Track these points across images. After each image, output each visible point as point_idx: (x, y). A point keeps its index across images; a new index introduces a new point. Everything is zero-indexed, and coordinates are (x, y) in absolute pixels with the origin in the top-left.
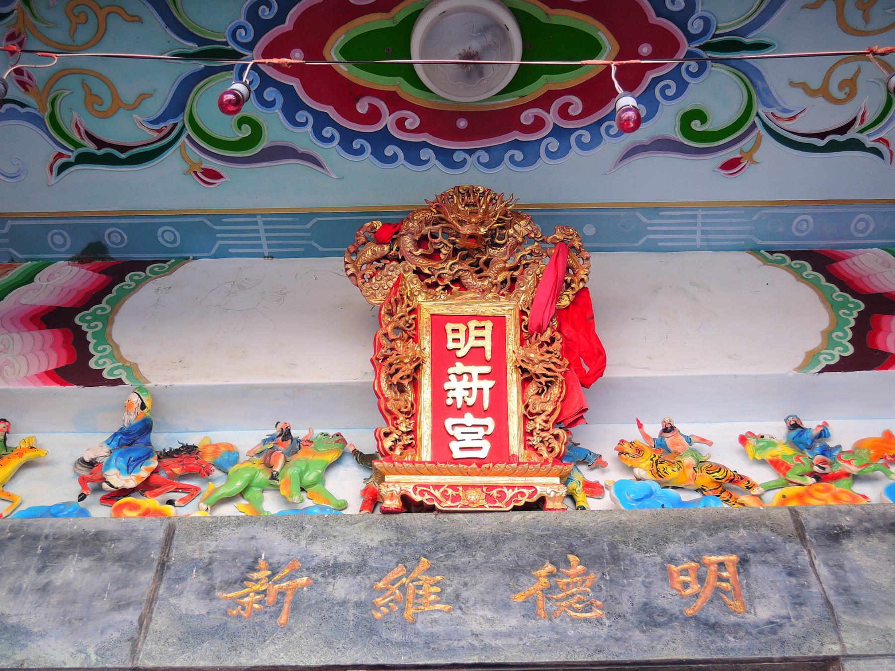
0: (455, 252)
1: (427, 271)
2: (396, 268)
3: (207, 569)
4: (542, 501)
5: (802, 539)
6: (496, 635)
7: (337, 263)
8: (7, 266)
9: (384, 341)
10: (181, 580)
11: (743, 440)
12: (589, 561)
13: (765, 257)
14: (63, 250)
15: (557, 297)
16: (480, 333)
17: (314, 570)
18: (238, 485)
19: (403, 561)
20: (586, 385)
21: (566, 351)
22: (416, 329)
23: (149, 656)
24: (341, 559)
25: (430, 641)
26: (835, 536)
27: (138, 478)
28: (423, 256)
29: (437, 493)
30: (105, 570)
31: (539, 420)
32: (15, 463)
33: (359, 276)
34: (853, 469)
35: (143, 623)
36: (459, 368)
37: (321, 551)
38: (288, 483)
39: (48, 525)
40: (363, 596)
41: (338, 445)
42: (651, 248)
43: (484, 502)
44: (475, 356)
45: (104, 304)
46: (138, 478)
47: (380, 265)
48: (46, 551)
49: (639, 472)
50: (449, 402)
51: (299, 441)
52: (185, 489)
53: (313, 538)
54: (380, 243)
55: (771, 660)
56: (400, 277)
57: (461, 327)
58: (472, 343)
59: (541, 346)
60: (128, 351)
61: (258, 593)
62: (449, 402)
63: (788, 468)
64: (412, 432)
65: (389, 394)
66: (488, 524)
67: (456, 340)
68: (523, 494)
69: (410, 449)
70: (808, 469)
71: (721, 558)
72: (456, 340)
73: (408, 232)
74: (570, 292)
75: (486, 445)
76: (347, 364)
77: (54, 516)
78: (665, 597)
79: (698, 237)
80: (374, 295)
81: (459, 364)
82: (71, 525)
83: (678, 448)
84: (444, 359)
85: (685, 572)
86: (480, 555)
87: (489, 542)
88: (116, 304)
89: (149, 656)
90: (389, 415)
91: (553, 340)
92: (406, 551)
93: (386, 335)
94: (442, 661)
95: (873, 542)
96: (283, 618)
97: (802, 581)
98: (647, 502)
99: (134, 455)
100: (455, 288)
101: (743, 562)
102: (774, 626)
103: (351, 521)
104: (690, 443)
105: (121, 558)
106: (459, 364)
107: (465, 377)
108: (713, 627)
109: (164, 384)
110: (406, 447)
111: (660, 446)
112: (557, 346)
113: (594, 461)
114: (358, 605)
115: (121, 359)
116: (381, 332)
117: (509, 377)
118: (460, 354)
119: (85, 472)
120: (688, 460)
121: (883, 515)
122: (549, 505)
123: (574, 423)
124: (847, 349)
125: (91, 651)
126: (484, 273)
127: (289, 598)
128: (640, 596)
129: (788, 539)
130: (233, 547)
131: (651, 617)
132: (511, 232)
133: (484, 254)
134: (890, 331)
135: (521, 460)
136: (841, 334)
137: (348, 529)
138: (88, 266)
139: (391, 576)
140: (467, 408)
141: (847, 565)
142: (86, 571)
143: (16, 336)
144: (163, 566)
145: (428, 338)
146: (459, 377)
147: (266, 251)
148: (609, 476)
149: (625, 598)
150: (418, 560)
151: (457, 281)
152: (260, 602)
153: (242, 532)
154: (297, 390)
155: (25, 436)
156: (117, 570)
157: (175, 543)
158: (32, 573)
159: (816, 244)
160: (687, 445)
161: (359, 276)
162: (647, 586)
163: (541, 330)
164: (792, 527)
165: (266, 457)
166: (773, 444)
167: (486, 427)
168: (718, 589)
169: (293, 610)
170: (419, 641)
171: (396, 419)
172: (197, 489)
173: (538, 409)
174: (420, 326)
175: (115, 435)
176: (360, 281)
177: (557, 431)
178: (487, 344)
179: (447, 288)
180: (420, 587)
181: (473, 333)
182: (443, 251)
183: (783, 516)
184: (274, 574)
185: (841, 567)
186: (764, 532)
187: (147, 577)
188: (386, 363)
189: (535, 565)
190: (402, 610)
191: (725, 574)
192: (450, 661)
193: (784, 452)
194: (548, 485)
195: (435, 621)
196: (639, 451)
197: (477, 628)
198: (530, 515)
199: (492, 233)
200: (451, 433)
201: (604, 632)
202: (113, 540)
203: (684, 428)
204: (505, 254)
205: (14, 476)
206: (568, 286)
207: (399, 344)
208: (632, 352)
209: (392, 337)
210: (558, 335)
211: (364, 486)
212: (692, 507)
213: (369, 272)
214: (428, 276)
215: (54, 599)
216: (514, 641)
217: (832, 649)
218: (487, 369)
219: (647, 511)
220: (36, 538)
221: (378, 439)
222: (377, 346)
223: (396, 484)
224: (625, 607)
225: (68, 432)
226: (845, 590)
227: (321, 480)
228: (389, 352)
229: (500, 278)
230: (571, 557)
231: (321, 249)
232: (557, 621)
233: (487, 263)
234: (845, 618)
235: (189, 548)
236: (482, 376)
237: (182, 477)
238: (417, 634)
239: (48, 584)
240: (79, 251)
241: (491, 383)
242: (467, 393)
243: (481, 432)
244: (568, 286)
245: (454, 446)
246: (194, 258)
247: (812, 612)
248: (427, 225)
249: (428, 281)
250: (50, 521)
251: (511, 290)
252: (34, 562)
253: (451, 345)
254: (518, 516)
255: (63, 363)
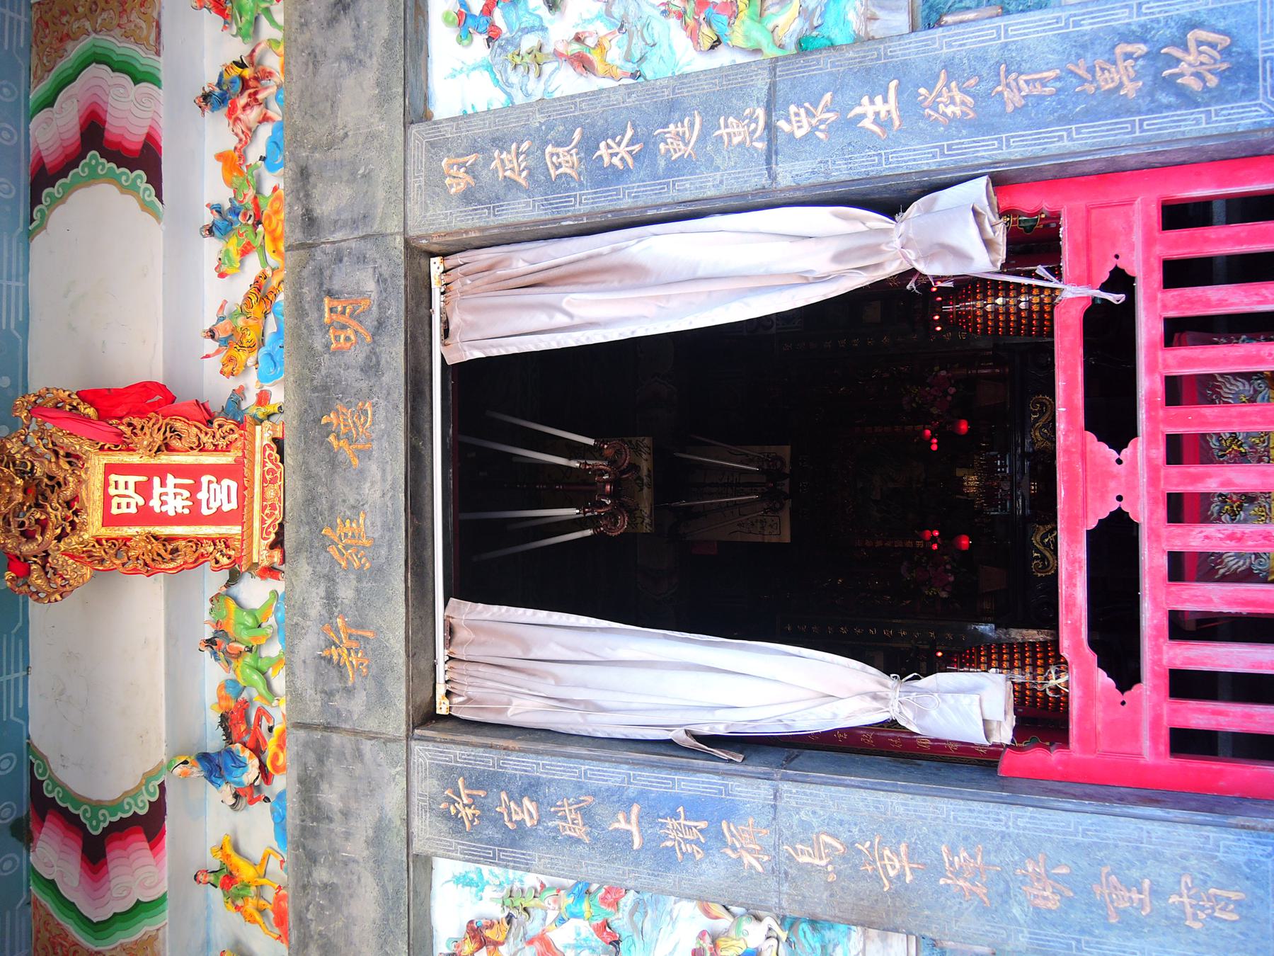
0: (38, 505)
1: (58, 531)
2: (55, 558)
3: (330, 694)
4: (275, 440)
5: (311, 246)
6: (384, 480)
7: (34, 608)
8: (36, 907)
9: (130, 566)
10: (339, 713)
11: (222, 275)
12: (327, 409)
13: (37, 227)
14: (18, 859)
15: (87, 419)
16: (122, 485)
17: (331, 613)
18: (256, 677)
19: (324, 548)
20: (174, 399)
21: (142, 414)
22: (117, 539)
23: (398, 728)
24: (323, 594)
25: (387, 528)
26: (310, 221)
27: (250, 757)
28: (42, 534)
29: (269, 522)
30: (330, 771)
31: (204, 439)
32: (236, 859)
33: (62, 590)
34: (251, 193)
35: (372, 736)
36: (155, 503)
37: (316, 609)
38: (255, 638)
39: (292, 820)
40: (352, 576)
41: (221, 599)
42: (24, 327)
43: (276, 486)
44: (144, 490)
45: (80, 812)
46: (250, 757)
47: (51, 571)
48: (314, 819)
49: (251, 362)
50: (186, 511)
51: (216, 632)
52: (259, 719)
53: (305, 616)
54: (29, 573)
55: (406, 286)
56: (64, 553)
57: (115, 501)
58: (131, 491)
59: (135, 434)
60: (129, 785)
61: (349, 654)
62: (186, 511)
63: (249, 243)
64: (214, 541)
65: (180, 561)
66: (295, 484)
67: (128, 505)
68: (270, 455)
69: (229, 542)
70: (250, 229)
71: (327, 310)
72: (128, 505)
73: (18, 547)
74: (81, 408)
75: (226, 482)
76: (146, 599)
77: (283, 818)
78: (357, 355)
79: (14, 284)
80: (82, 576)
81: (151, 503)
82: (292, 803)
83: (229, 328)
84: (145, 516)
85: (337, 338)
86: (320, 489)
87: (310, 482)
88: (79, 800)
89: (398, 728)
90: (197, 562)
91: (130, 425)
92: (316, 545)
93: (123, 565)
94: (403, 518)
95: (316, 193)
96: (369, 634)
97: (346, 253)
98: (277, 359)
99: (230, 764)
100: (76, 506)
101: (330, 293)
102: (380, 280)
103: (291, 587)
104: (224, 318)
105: (320, 761)
106: (151, 503)
107: (163, 498)
108: (381, 324)
109: (164, 748)
110: (227, 546)
111: (226, 342)
112: (136, 421)
113: (239, 394)
114: (359, 580)
115: (138, 788)
116: (121, 569)
117: (164, 462)
118: (141, 502)
119: (244, 801)
120: (240, 322)
121: (294, 181)
122: (279, 435)
123: (207, 411)
124: (139, 176)
125: (393, 771)
126: (61, 480)
127: (354, 631)
128: (358, 374)
129: (312, 257)
130: (311, 676)
131: (372, 367)
132: (18, 456)
133: (41, 481)
134: (122, 136)
135: (240, 454)
136: (124, 178)
137: (298, 590)
138: (35, 834)
139: (337, 556)
140: (193, 497)
141: (334, 217)
142: (331, 785)
143: (114, 882)
144: (327, 728)
145: (125, 529)
146: (163, 503)
147: (22, 673)
148: (252, 384)
149: (357, 385)
150: (324, 536)
151: (69, 504)
152: (357, 653)
153: (299, 671)
154: (170, 635)
155: (209, 855)
156: (330, 763)
157: (308, 721)
158: (332, 826)
159: (24, 179)
160: (227, 321)
161: (62, 590)
162: (347, 367)
163: (121, 434)
164: (302, 252)
165: (231, 657)
166: (227, 252)
167: (210, 482)
168: (351, 315)
169: (363, 627)
170: (387, 536)
171: (202, 555)
172: (259, 710)
173: (195, 440)
174: (114, 536)
175: (212, 782)
176: (68, 588)
177: (216, 425)
178: (132, 479)
179: (76, 513)
180: (346, 535)
181: (121, 491)
182: (38, 516)
183: (293, 257)
184: (334, 644)
185: (336, 222)
186: (305, 273)
187: (336, 739)
188: (152, 564)
189: (330, 448)
190: (364, 547)
191: (339, 309)
192: (403, 514)
193: (234, 244)
194: (262, 436)
195: (372, 524)
196: (230, 359)
197: (379, 494)
198: (287, 450)
199: (21, 474)
200: (214, 510)
201: (382, 403)
202: (306, 769)
203: (209, 321)
204: (42, 463)
205: (247, 858)
206: (75, 408)
207: (132, 553)
208: (138, 357)
209: (126, 559)
210: (125, 420)
211: (258, 579)
212: (283, 325)
213: (59, 581)
214: (63, 529)
215: (353, 805)
216: (388, 468)
217: (399, 241)
218: (156, 480)
219: (286, 360)
220: (304, 829)
221: (221, 568)
222: (135, 571)
223: (260, 552)
224: (364, 385)
225: (209, 822)
226: (355, 223)
227: (252, 612)
228: (141, 562)
229: (67, 467)
230: (323, 422)
231: (20, 624)
232: (374, 436)
233: (51, 478)
234: (376, 228)
235: (312, 709)
236: (163, 484)
237: (248, 722)
238: (382, 537)
239: (342, 812)
240: (20, 844)
241: (170, 477)
242: (179, 497)
243: (213, 486)
244: (75, 408)
245: (226, 508)
246: (28, 738)
247: (370, 250)
248: (10, 531)
249: (68, 529)
250: (289, 820)
251: (78, 457)
252: (324, 826)
253: (133, 510)
254: (288, 459)
255: (143, 836)
